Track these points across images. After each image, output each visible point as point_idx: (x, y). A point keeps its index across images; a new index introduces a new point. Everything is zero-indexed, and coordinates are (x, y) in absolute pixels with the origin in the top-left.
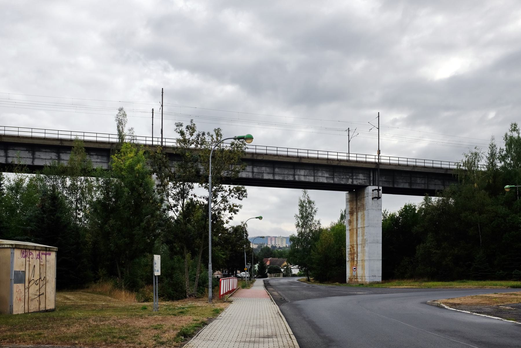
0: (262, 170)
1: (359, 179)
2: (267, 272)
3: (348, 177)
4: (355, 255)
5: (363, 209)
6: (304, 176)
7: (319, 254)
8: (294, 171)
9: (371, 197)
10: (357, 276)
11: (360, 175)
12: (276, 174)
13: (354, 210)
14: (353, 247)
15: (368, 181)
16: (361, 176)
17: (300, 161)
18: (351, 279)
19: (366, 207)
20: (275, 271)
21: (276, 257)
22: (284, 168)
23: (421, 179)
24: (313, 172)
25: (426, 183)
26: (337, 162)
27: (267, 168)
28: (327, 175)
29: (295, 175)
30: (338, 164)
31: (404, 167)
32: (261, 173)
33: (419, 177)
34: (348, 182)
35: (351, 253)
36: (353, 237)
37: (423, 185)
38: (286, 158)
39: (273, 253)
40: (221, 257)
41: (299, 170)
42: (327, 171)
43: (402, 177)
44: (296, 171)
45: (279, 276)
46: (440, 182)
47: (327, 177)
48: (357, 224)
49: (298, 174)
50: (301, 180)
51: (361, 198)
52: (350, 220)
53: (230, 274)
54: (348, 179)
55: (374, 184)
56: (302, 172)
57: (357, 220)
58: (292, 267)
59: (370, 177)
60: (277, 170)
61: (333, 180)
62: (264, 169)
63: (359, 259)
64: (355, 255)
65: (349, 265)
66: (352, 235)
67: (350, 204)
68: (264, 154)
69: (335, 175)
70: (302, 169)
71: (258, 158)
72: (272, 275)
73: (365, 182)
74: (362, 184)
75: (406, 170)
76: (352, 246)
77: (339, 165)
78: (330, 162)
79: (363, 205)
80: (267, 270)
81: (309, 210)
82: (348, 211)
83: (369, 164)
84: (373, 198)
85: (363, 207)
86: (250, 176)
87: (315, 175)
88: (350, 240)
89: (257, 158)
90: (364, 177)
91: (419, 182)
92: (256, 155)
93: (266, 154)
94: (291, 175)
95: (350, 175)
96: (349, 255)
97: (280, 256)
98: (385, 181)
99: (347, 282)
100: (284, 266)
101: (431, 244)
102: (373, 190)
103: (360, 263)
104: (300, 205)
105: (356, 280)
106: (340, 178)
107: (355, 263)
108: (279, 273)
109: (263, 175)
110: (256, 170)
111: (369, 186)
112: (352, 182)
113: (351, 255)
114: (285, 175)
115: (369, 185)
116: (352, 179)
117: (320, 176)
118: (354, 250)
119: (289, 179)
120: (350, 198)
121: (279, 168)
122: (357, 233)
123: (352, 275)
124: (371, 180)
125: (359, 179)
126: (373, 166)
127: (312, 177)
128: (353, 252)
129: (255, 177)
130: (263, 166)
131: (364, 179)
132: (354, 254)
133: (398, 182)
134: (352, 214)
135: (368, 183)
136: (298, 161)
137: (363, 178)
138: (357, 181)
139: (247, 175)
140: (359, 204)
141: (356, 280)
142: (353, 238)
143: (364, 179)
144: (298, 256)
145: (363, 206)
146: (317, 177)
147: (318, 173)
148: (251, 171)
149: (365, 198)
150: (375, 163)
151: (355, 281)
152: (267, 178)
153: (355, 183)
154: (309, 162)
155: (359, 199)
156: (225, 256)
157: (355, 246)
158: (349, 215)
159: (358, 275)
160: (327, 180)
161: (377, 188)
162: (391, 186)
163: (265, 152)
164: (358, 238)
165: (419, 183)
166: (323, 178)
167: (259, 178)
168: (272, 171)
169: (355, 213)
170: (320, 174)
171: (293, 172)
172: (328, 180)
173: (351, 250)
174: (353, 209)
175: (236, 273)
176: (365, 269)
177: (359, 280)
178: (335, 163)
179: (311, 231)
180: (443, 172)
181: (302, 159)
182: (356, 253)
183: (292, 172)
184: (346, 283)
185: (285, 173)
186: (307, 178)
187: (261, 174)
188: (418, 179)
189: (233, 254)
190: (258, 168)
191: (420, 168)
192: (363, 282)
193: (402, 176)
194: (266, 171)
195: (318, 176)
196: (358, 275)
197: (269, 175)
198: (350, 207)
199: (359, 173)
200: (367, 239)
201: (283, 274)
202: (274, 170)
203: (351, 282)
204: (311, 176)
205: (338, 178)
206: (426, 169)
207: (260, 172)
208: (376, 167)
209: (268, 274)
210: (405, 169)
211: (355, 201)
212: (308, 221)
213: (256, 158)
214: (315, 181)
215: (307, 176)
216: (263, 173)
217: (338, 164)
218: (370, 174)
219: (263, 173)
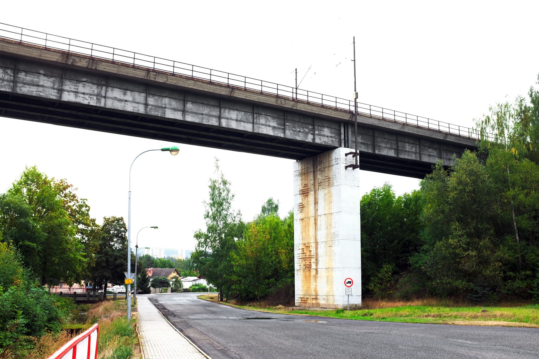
0: (163, 102)
1: (324, 136)
2: (150, 285)
3: (307, 130)
4: (313, 260)
5: (327, 185)
6: (237, 120)
7: (247, 258)
8: (220, 112)
9: (344, 165)
10: (316, 295)
11: (324, 129)
12: (187, 112)
13: (309, 187)
14: (308, 247)
15: (337, 140)
16: (326, 131)
17: (231, 94)
18: (304, 300)
19: (335, 182)
20: (162, 284)
21: (158, 267)
22: (202, 103)
23: (411, 146)
24: (251, 117)
25: (418, 151)
26: (292, 103)
27: (171, 100)
28: (274, 123)
29: (222, 118)
30: (293, 106)
31: (390, 124)
32: (162, 107)
33: (408, 143)
34: (307, 138)
35: (304, 257)
36: (308, 231)
37: (414, 155)
38: (208, 86)
39: (154, 263)
40: (80, 260)
41: (227, 110)
42: (274, 118)
43: (386, 140)
44: (222, 111)
45: (166, 291)
46: (435, 153)
47: (274, 128)
48: (316, 210)
49: (226, 117)
50: (231, 127)
51: (324, 168)
52: (302, 203)
53: (96, 287)
54: (307, 134)
55: (346, 145)
56: (234, 114)
57: (316, 203)
58: (182, 280)
59: (340, 135)
60: (189, 106)
61: (284, 133)
62: (166, 101)
63: (320, 266)
64: (313, 260)
65: (301, 275)
66: (307, 227)
67: (302, 179)
68: (169, 74)
69: (287, 125)
70: (234, 110)
71: (157, 80)
72: (158, 289)
73: (332, 141)
74: (328, 144)
75: (393, 128)
76: (307, 245)
77: (295, 108)
78: (281, 101)
79: (327, 178)
80: (150, 283)
81: (224, 194)
82: (298, 190)
83: (340, 113)
84: (346, 167)
85: (328, 182)
86: (141, 110)
87: (255, 121)
88: (302, 236)
89: (155, 78)
90: (331, 133)
91: (408, 150)
92: (155, 74)
93: (173, 74)
94: (215, 116)
95: (310, 127)
96: (301, 260)
97: (163, 266)
98: (361, 143)
99: (296, 304)
100: (173, 278)
101: (459, 241)
102: (346, 155)
103: (322, 273)
104: (210, 187)
105: (314, 302)
106: (295, 131)
107: (313, 272)
108: (167, 287)
109: (165, 111)
110: (151, 101)
111: (339, 147)
112: (314, 139)
113: (304, 259)
114: (204, 116)
115: (338, 146)
116: (314, 134)
117: (262, 125)
118: (310, 251)
119: (210, 123)
120: (302, 169)
121: (192, 102)
122: (316, 224)
123: (306, 293)
124: (343, 139)
125: (324, 136)
126: (347, 117)
127: (249, 124)
128: (308, 254)
129: (149, 113)
130: (166, 97)
131: (331, 137)
132: (310, 257)
133: (380, 146)
134: (305, 194)
135: (338, 143)
136: (227, 94)
137: (329, 135)
138: (320, 139)
139: (134, 107)
140: (319, 176)
141: (314, 302)
142: (307, 232)
143: (331, 137)
144: (208, 263)
145: (327, 180)
146: (258, 126)
147: (259, 119)
148: (143, 102)
149: (331, 168)
150: (350, 112)
151: (313, 304)
152: (171, 117)
153: (318, 141)
154: (246, 97)
155: (320, 169)
156: (87, 259)
157: (313, 245)
158: (301, 195)
159: (320, 293)
160: (274, 132)
161: (354, 151)
162: (370, 151)
163: (170, 69)
164: (319, 233)
165: (409, 151)
166: (268, 128)
167: (157, 115)
168: (181, 107)
169: (313, 193)
170: (262, 121)
171: (218, 113)
172: (275, 132)
173: (303, 251)
174: (308, 186)
175: (106, 286)
176: (333, 284)
177: (322, 302)
178: (289, 105)
179: (226, 225)
180: (442, 138)
181: (236, 91)
182: (315, 256)
183: (215, 112)
184: (293, 305)
185: (204, 113)
186: (241, 126)
187: (161, 109)
188: (407, 145)
189: (102, 258)
190: (155, 99)
191: (412, 128)
192: (329, 305)
193: (385, 138)
194: (170, 105)
195: (259, 124)
196: (318, 292)
197: (176, 113)
198: (302, 184)
199: (323, 127)
200: (336, 233)
201: (172, 288)
202: (184, 106)
203: (304, 305)
204: (248, 123)
205: (291, 131)
206: (419, 130)
207: (160, 105)
208: (350, 118)
209: (152, 289)
210: (391, 128)
211: (312, 173)
212: (222, 210)
213: (153, 79)
214: (255, 131)
215: (240, 121)
216: (165, 107)
217: (293, 106)
218: (341, 130)
219: (165, 107)
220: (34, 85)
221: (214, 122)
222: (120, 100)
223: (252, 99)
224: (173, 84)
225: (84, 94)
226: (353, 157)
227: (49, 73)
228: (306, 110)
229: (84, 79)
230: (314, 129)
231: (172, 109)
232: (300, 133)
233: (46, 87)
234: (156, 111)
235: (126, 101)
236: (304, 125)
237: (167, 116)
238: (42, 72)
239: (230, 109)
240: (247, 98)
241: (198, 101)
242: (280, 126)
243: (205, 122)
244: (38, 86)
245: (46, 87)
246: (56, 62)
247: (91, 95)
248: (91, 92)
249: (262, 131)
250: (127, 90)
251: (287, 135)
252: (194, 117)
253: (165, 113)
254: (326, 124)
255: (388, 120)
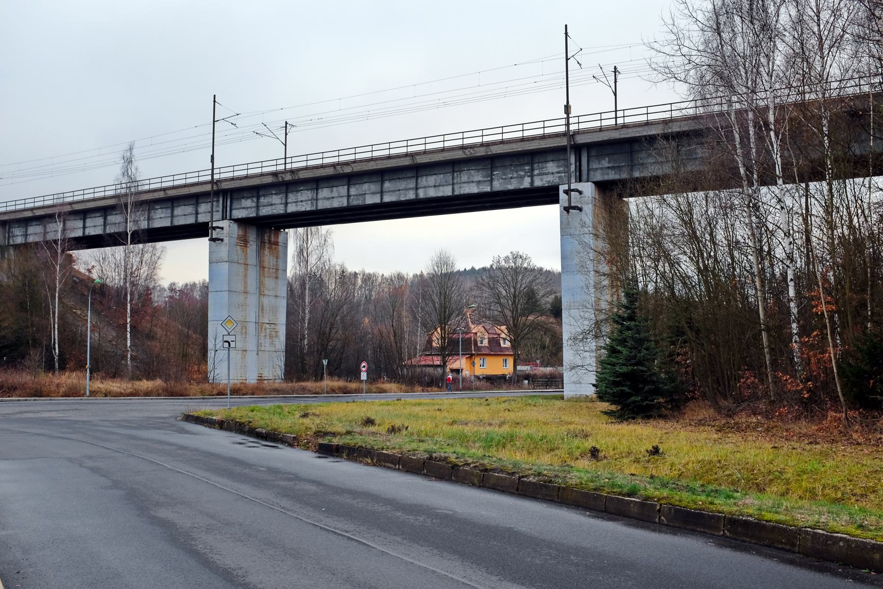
12: (385, 192)
22: (399, 178)
31: (640, 129)
34: (522, 184)
41: (425, 177)
47: (479, 182)
54: (522, 177)
56: (431, 180)
69: (494, 175)
74: (553, 184)
78: (469, 151)
90: (558, 167)
95: (526, 168)
106: (506, 179)
112: (532, 182)
114: (401, 192)
117: (464, 183)
119: (407, 198)
121: (390, 180)
131: (558, 172)
136: (411, 163)
137: (556, 170)
138: (542, 180)
143: (558, 172)
147: (461, 177)
160: (478, 188)
166: (470, 185)
183: (412, 184)
194: (369, 189)
199: (546, 162)
204: (447, 185)
205: (501, 181)
216: (365, 194)
219: (365, 194)
220: (269, 206)
221: (411, 196)
222: (328, 199)
223: (438, 160)
224: (358, 170)
225: (302, 201)
226: (215, 230)
227: (278, 192)
228: (505, 151)
229: (302, 188)
230: (532, 170)
231: (371, 193)
232: (512, 180)
233: (277, 204)
234: (358, 199)
235: (333, 198)
236: (518, 168)
237: (367, 203)
238: (274, 192)
239: (427, 175)
240: (432, 161)
241: (394, 178)
242: (487, 178)
243: (403, 198)
244: (272, 205)
245: (277, 204)
246: (273, 182)
247: (307, 201)
248: (306, 199)
249: (464, 190)
250: (333, 187)
251: (496, 186)
252: (391, 195)
253: (365, 200)
254: (550, 157)
255: (632, 126)
